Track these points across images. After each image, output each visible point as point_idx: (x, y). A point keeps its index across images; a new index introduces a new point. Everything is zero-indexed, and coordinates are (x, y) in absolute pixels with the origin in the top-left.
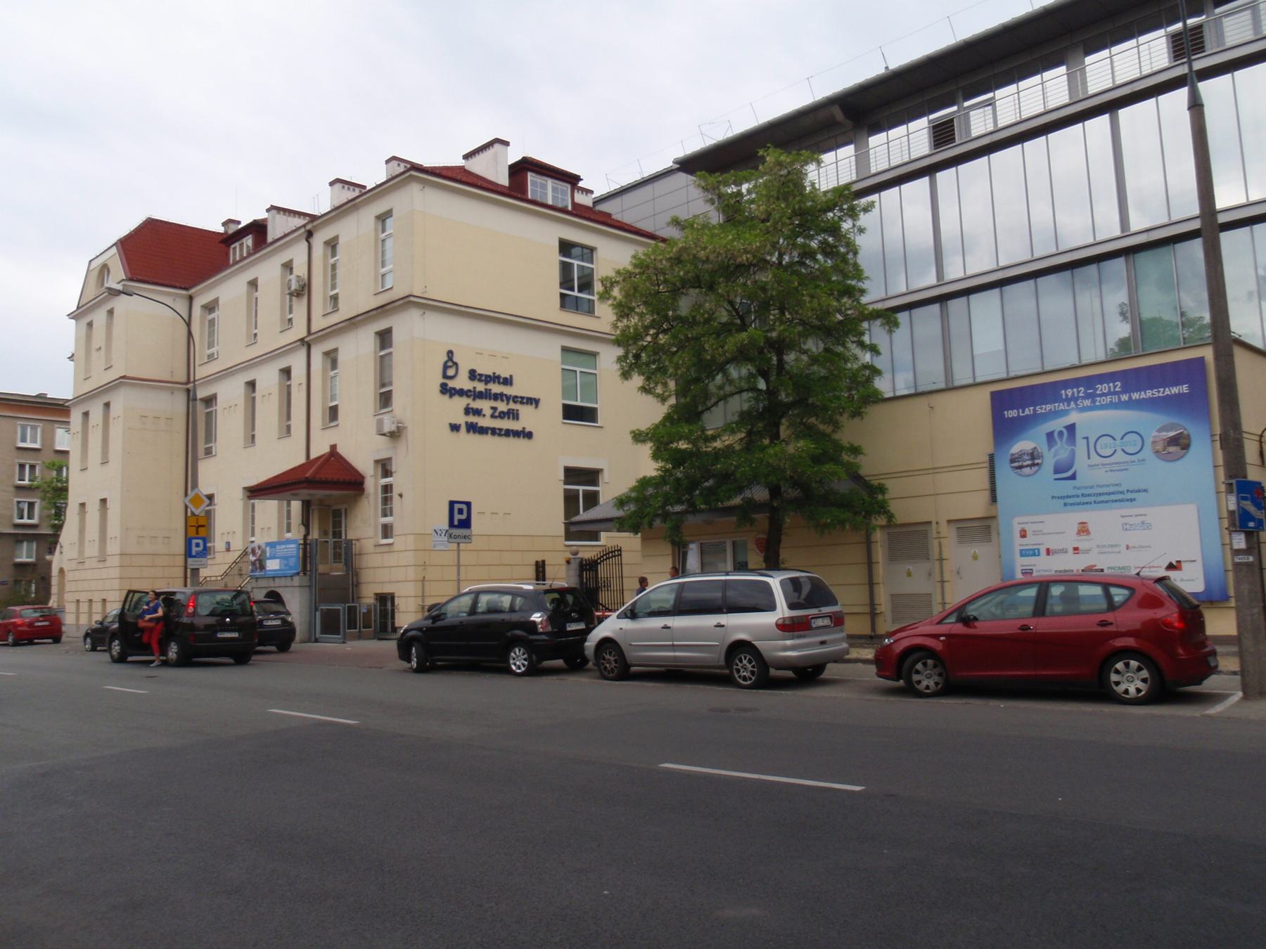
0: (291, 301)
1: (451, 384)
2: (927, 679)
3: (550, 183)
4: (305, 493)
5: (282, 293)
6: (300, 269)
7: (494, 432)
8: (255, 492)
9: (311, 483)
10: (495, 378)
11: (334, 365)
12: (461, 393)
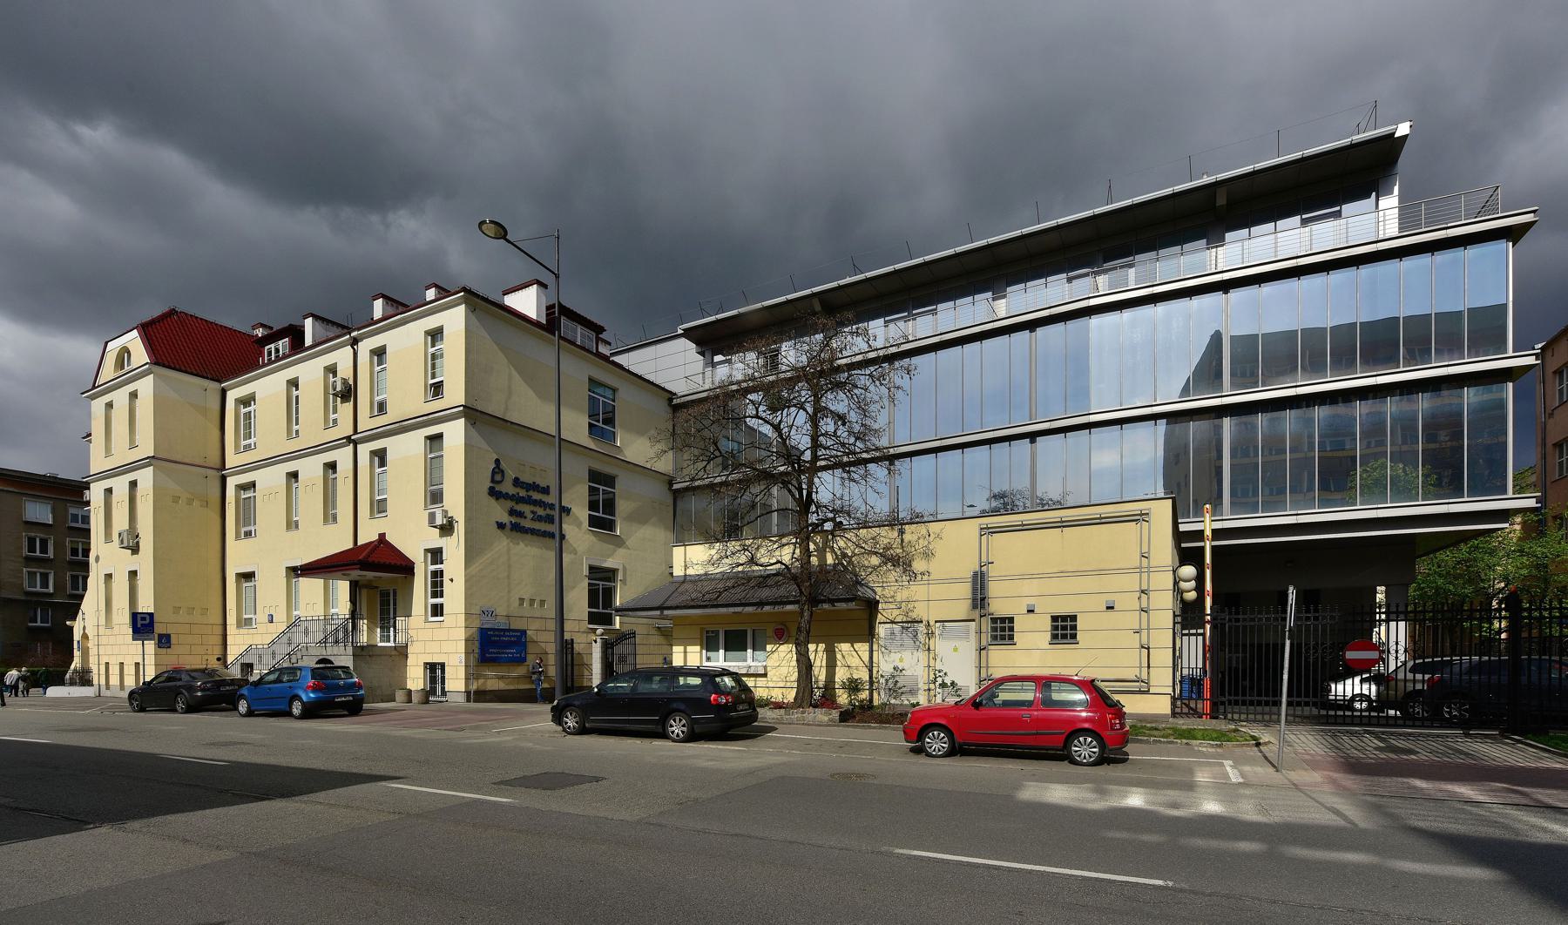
0: (335, 401)
1: (498, 488)
2: (937, 742)
3: (579, 329)
4: (356, 574)
5: (326, 393)
6: (345, 371)
7: (533, 532)
8: (298, 571)
9: (365, 565)
10: (534, 487)
11: (383, 463)
12: (506, 496)
